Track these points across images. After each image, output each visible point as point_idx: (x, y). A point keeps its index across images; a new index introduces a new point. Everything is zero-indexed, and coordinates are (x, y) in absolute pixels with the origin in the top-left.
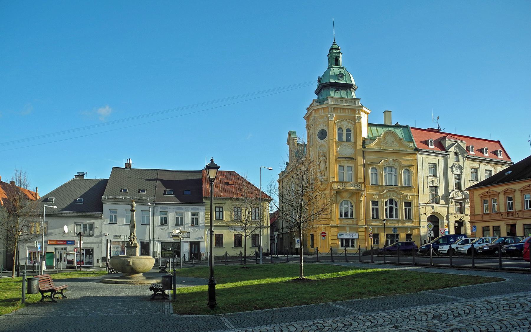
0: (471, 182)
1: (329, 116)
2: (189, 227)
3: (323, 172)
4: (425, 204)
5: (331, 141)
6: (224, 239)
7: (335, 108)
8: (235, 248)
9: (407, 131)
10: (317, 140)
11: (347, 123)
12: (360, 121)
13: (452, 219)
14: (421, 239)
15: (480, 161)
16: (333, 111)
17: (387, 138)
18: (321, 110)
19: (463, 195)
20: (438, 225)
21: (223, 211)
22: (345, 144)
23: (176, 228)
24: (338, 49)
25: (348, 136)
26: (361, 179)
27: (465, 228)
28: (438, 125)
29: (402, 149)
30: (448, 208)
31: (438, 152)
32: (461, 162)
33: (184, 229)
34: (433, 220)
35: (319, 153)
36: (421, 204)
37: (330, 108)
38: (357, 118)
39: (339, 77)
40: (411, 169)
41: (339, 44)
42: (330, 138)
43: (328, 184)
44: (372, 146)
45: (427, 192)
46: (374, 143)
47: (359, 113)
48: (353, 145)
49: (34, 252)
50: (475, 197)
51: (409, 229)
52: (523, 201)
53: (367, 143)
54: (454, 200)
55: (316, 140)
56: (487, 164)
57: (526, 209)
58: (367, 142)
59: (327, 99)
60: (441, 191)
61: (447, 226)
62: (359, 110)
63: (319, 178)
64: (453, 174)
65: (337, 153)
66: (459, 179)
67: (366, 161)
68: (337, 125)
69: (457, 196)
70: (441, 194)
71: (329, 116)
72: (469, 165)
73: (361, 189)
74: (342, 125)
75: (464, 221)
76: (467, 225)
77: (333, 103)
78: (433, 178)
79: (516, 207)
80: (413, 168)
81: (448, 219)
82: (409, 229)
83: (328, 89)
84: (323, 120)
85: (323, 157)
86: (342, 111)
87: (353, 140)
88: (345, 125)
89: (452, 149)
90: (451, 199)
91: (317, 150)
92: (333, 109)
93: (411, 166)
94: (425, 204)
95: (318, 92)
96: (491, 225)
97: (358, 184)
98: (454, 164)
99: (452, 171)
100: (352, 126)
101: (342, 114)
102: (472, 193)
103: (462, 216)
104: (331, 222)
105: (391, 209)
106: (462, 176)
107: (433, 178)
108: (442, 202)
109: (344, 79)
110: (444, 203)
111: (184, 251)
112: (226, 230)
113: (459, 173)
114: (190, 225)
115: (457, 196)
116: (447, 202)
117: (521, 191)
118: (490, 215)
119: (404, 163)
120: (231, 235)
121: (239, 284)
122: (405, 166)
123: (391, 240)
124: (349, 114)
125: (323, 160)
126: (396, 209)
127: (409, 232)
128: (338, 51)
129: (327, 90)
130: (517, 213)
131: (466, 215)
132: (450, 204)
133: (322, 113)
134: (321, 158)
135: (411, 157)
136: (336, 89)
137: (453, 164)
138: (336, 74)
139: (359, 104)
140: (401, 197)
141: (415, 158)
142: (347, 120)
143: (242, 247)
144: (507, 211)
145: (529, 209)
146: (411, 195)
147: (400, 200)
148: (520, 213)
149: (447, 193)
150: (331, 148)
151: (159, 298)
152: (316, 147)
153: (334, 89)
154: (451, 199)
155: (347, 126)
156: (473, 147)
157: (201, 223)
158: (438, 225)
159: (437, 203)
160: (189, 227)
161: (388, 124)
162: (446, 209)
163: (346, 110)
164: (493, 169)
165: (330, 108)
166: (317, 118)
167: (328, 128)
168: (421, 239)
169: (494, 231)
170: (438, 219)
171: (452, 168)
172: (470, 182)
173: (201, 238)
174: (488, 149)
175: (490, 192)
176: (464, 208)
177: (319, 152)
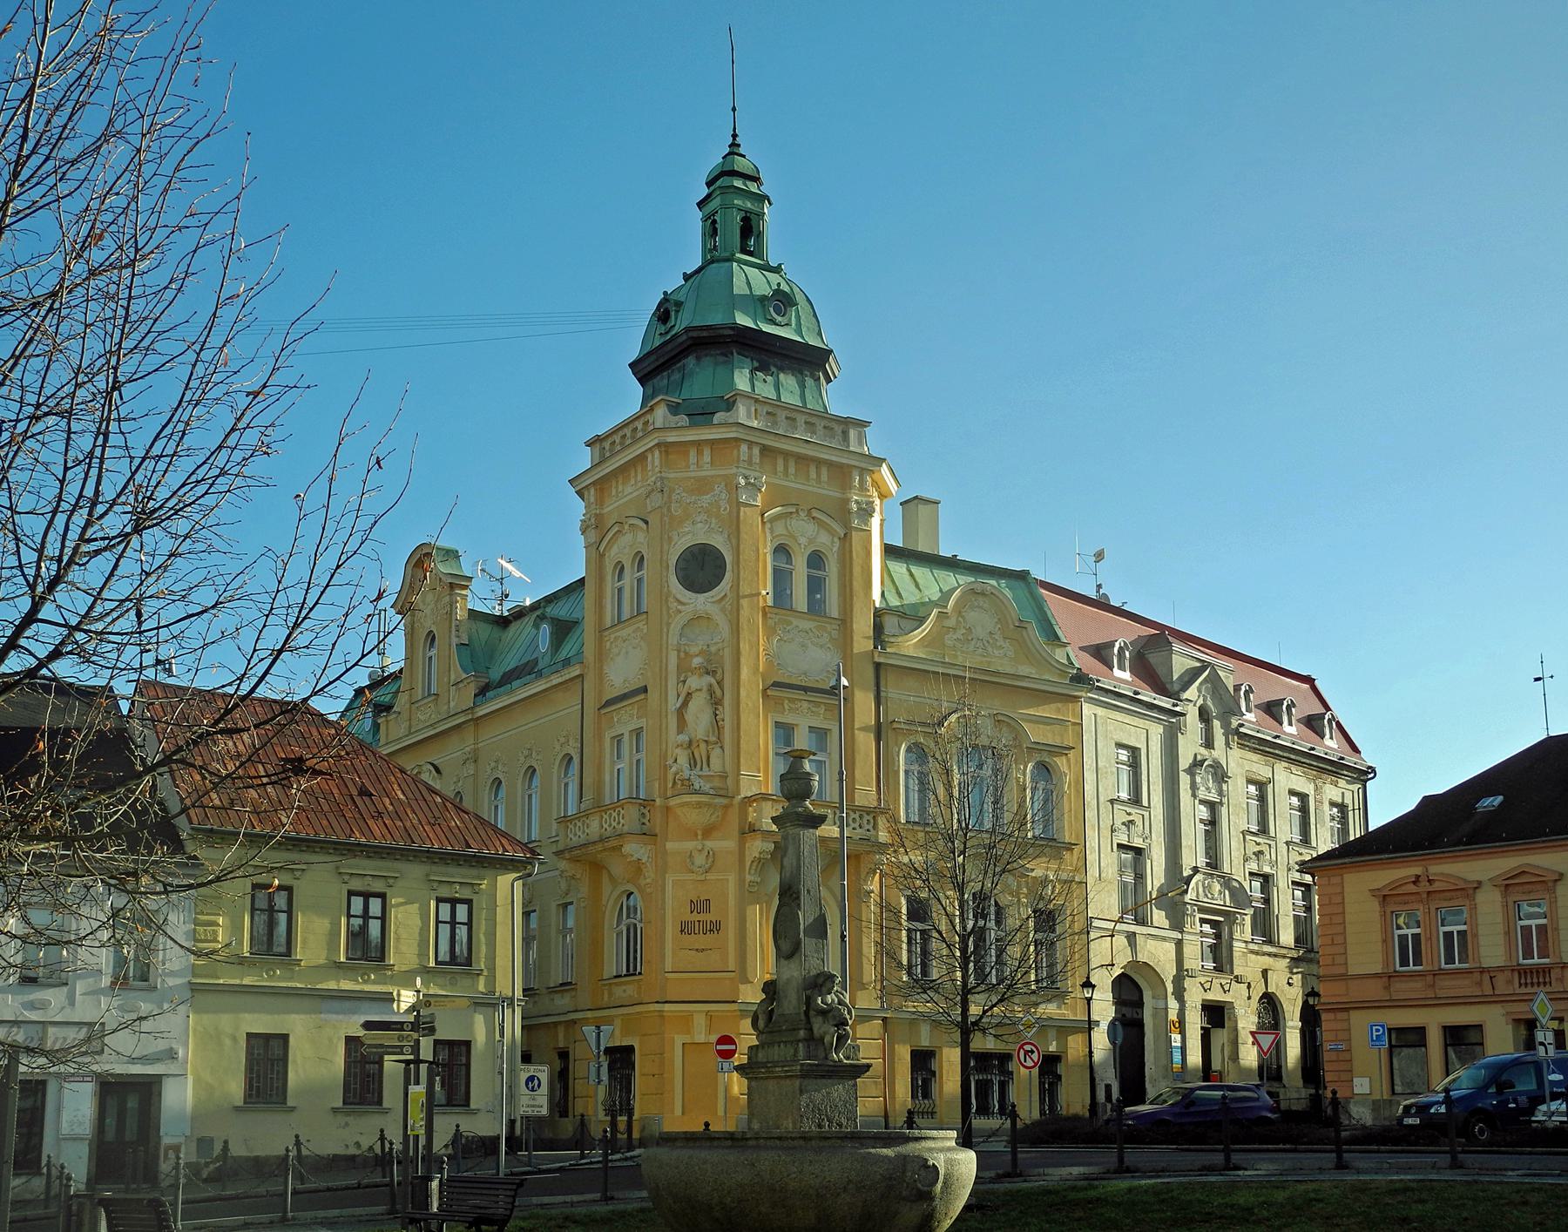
0: (1248, 837)
1: (742, 482)
2: (101, 991)
3: (703, 746)
4: (1111, 925)
5: (744, 602)
6: (295, 1062)
7: (765, 450)
8: (348, 1114)
9: (1028, 595)
10: (674, 591)
11: (811, 528)
12: (866, 525)
13: (1195, 997)
14: (1092, 1080)
15: (1277, 752)
16: (756, 459)
17: (972, 616)
18: (700, 453)
19: (1227, 892)
20: (1140, 1016)
21: (290, 913)
22: (806, 624)
23: (20, 998)
24: (756, 179)
25: (815, 585)
26: (866, 794)
27: (1232, 1036)
28: (1099, 586)
29: (1024, 670)
30: (1179, 944)
31: (1151, 697)
32: (1219, 752)
33: (72, 1003)
34: (1124, 997)
35: (682, 655)
36: (1096, 923)
37: (744, 448)
38: (854, 507)
39: (771, 309)
40: (1061, 762)
41: (752, 156)
42: (745, 589)
43: (726, 807)
44: (911, 644)
45: (1110, 871)
46: (923, 631)
47: (863, 488)
48: (835, 634)
50: (1346, 901)
51: (1052, 1033)
52: (1389, 935)
53: (893, 631)
54: (1202, 910)
55: (669, 593)
56: (1293, 768)
57: (1443, 966)
58: (890, 623)
59: (729, 405)
60: (1156, 875)
61: (1177, 1025)
62: (863, 471)
63: (686, 773)
64: (1195, 798)
65: (769, 663)
66: (1343, 818)
67: (886, 714)
68: (771, 530)
69: (1209, 896)
70: (1157, 884)
71: (742, 482)
72: (1242, 766)
73: (877, 835)
74: (792, 536)
75: (1227, 1007)
76: (1239, 1022)
77: (755, 424)
78: (1129, 810)
79: (1483, 951)
80: (1068, 760)
81: (1179, 994)
82: (1052, 1033)
83: (721, 359)
84: (706, 499)
85: (701, 676)
86: (792, 470)
87: (833, 610)
88: (806, 535)
89: (1191, 693)
90: (1189, 907)
91: (673, 640)
92: (756, 451)
93: (1056, 750)
94: (1111, 925)
95: (650, 369)
96: (1434, 1021)
98: (1199, 758)
99: (1194, 787)
100: (833, 542)
101: (792, 485)
102: (1335, 880)
103: (1224, 982)
104: (742, 987)
106: (1224, 810)
107: (1129, 810)
108: (1159, 917)
109: (790, 319)
110: (1166, 924)
111: (65, 1129)
112: (302, 1016)
113: (1213, 796)
114: (106, 981)
115: (1209, 896)
116: (1177, 924)
117: (1503, 889)
118: (1385, 979)
119: (1035, 734)
120: (330, 1040)
122: (1036, 748)
123: (977, 1082)
124: (820, 487)
125: (705, 689)
127: (1053, 1048)
128: (753, 187)
129: (716, 364)
130: (1491, 978)
131: (1236, 977)
132: (1187, 928)
133: (703, 466)
134: (694, 682)
135: (1058, 710)
136: (756, 364)
137: (1196, 755)
138: (757, 292)
139: (860, 444)
140: (1019, 887)
141: (1073, 715)
142: (815, 514)
143: (386, 1104)
144: (1519, 965)
145: (1411, 967)
147: (1019, 900)
148: (1501, 979)
149: (1177, 879)
150: (745, 634)
152: (669, 624)
153: (749, 360)
154: (1189, 907)
155: (811, 541)
156: (1252, 692)
157: (172, 974)
158: (1140, 1016)
159: (1141, 921)
160: (101, 991)
161: (922, 547)
162: (1171, 947)
163: (808, 466)
164: (1313, 792)
165: (744, 448)
166: (672, 490)
167: (734, 541)
168: (1092, 1080)
169: (1449, 1048)
170: (1141, 991)
171: (1191, 771)
172: (1244, 838)
173: (171, 1055)
174: (1294, 706)
175: (1429, 881)
176: (1231, 946)
177: (679, 651)
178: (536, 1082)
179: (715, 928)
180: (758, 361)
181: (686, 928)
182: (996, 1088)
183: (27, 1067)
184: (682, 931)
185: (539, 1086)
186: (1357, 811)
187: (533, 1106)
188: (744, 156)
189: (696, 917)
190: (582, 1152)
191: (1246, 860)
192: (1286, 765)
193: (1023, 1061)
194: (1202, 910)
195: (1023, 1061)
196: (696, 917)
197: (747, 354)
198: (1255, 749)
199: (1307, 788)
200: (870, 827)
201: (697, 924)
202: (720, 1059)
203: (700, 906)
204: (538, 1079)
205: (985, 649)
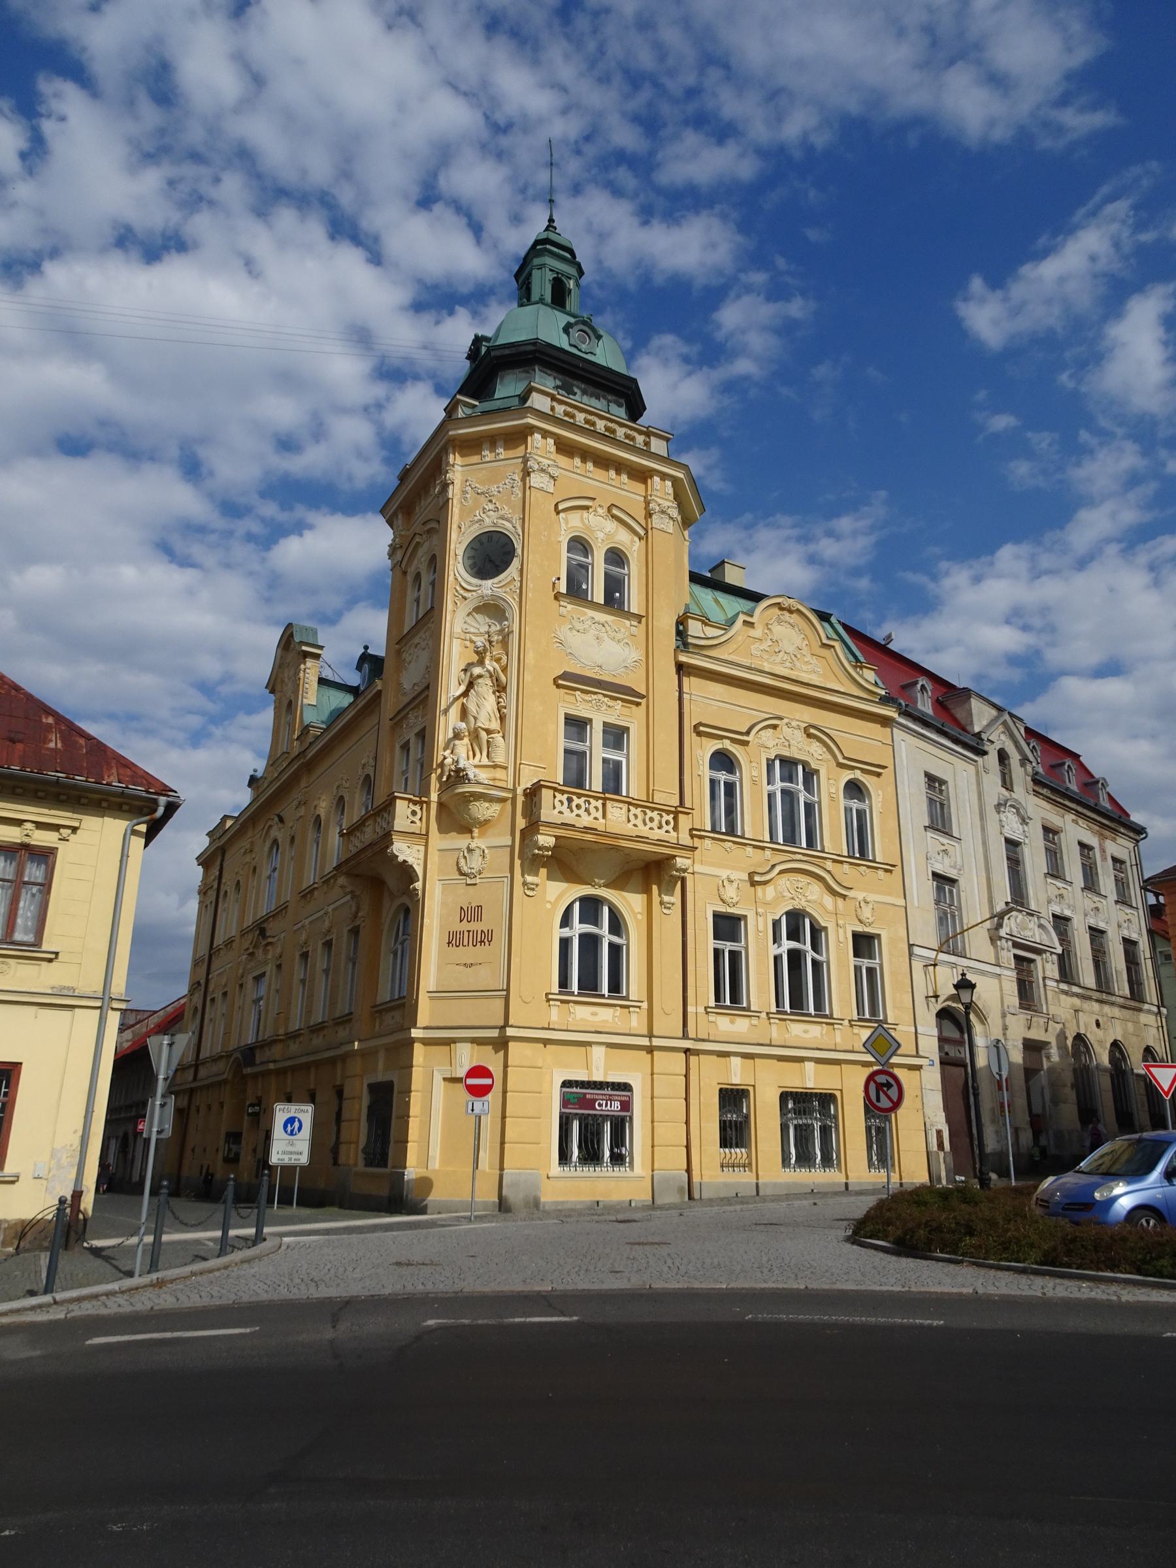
49: (311, 1031)
54: (1016, 945)
56: (1080, 821)
94: (932, 954)
97: (570, 800)
105: (590, 943)
121: (168, 1335)
126: (615, 950)
136: (558, 383)
146: (489, 848)
151: (930, 1045)
178: (297, 1124)
179: (485, 938)
180: (560, 380)
181: (454, 940)
182: (817, 1134)
183: (1094, 1119)
184: (449, 943)
185: (300, 1129)
186: (1134, 867)
187: (291, 1153)
188: (560, 235)
189: (465, 926)
190: (259, 1231)
191: (1049, 902)
192: (1074, 817)
193: (873, 1098)
194: (1016, 945)
195: (873, 1098)
196: (465, 926)
197: (549, 372)
198: (1048, 797)
199: (1092, 840)
200: (670, 828)
201: (466, 934)
202: (471, 1098)
203: (472, 913)
204: (300, 1121)
205: (792, 662)
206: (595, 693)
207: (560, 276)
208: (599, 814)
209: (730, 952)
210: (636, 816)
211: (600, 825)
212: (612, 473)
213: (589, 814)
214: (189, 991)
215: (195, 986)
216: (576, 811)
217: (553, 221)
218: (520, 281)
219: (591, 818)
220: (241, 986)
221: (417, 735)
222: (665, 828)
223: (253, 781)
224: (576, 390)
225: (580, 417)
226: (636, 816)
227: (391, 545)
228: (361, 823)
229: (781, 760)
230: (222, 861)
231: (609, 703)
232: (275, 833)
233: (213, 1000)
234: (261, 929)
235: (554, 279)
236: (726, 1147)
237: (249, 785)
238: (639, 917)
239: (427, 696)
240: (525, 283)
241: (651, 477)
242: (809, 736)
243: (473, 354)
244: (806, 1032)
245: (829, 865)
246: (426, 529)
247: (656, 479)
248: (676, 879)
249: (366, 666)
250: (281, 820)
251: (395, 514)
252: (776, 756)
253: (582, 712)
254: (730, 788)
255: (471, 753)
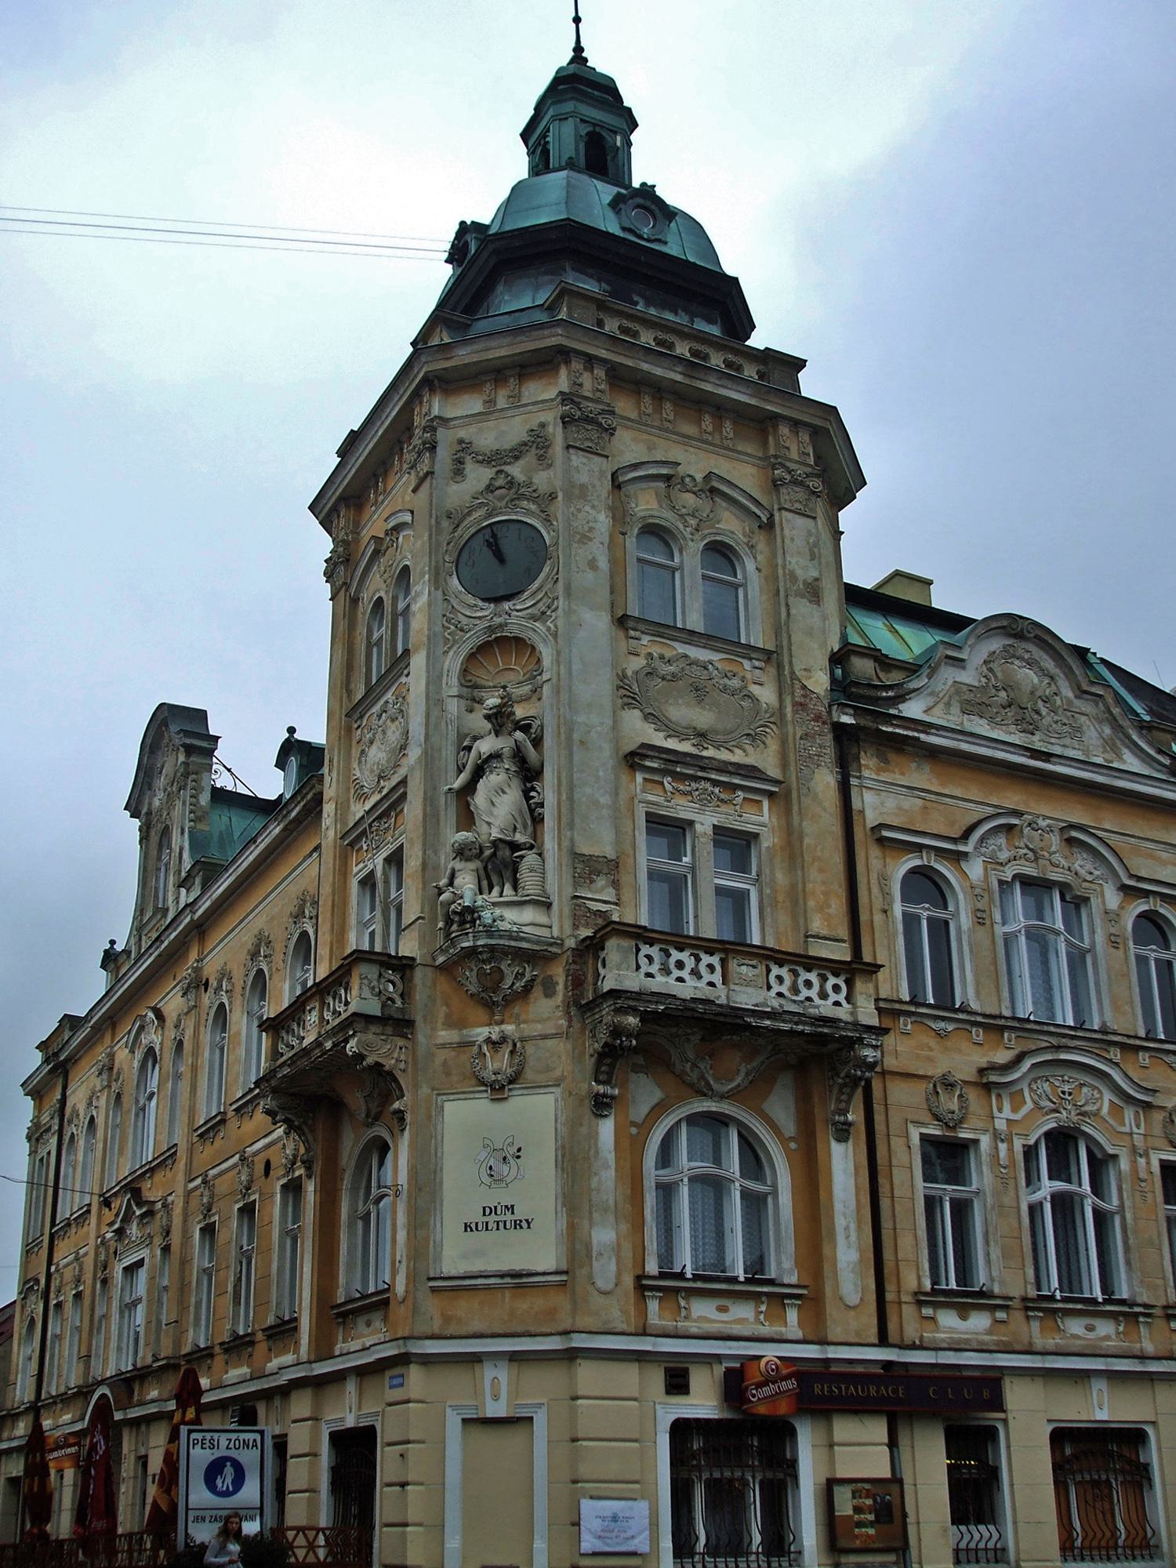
200: (841, 997)
206: (696, 779)
207: (598, 129)
208: (717, 978)
209: (952, 1201)
210: (780, 979)
211: (720, 995)
212: (708, 423)
213: (700, 977)
214: (20, 1293)
215: (28, 1286)
216: (676, 973)
217: (582, 50)
218: (531, 143)
219: (702, 984)
220: (104, 1282)
221: (388, 860)
222: (833, 997)
223: (110, 959)
224: (636, 298)
225: (647, 338)
226: (780, 979)
227: (330, 558)
228: (297, 1009)
229: (1022, 883)
230: (65, 1088)
231: (722, 796)
232: (152, 1037)
233: (59, 1305)
234: (133, 1188)
235: (588, 134)
236: (966, 1523)
237: (104, 966)
238: (793, 1145)
239: (405, 794)
240: (539, 144)
241: (775, 427)
242: (1070, 841)
243: (456, 254)
244: (1090, 1328)
245: (1115, 1054)
246: (390, 526)
247: (784, 430)
248: (856, 1081)
249: (293, 762)
250: (160, 1016)
251: (335, 509)
252: (1015, 877)
253: (682, 808)
254: (940, 930)
255: (485, 883)
